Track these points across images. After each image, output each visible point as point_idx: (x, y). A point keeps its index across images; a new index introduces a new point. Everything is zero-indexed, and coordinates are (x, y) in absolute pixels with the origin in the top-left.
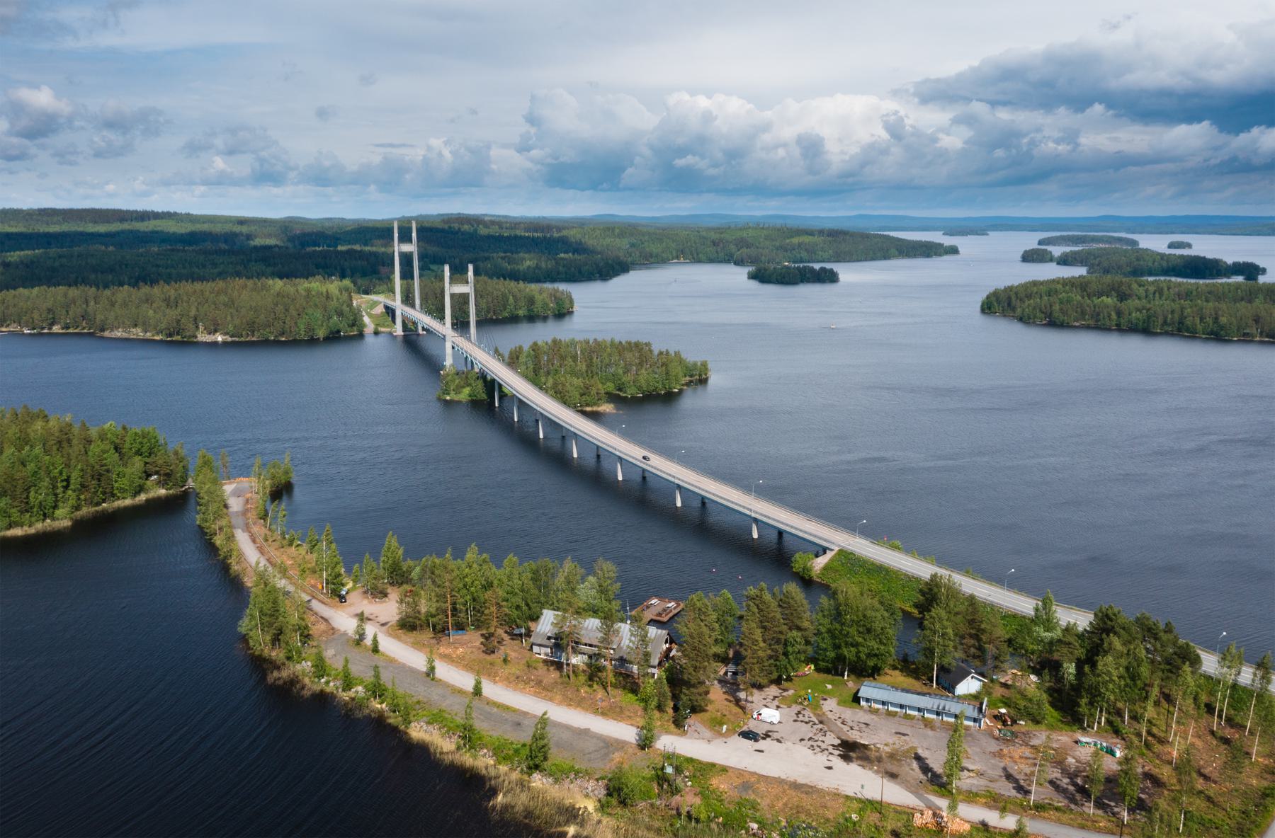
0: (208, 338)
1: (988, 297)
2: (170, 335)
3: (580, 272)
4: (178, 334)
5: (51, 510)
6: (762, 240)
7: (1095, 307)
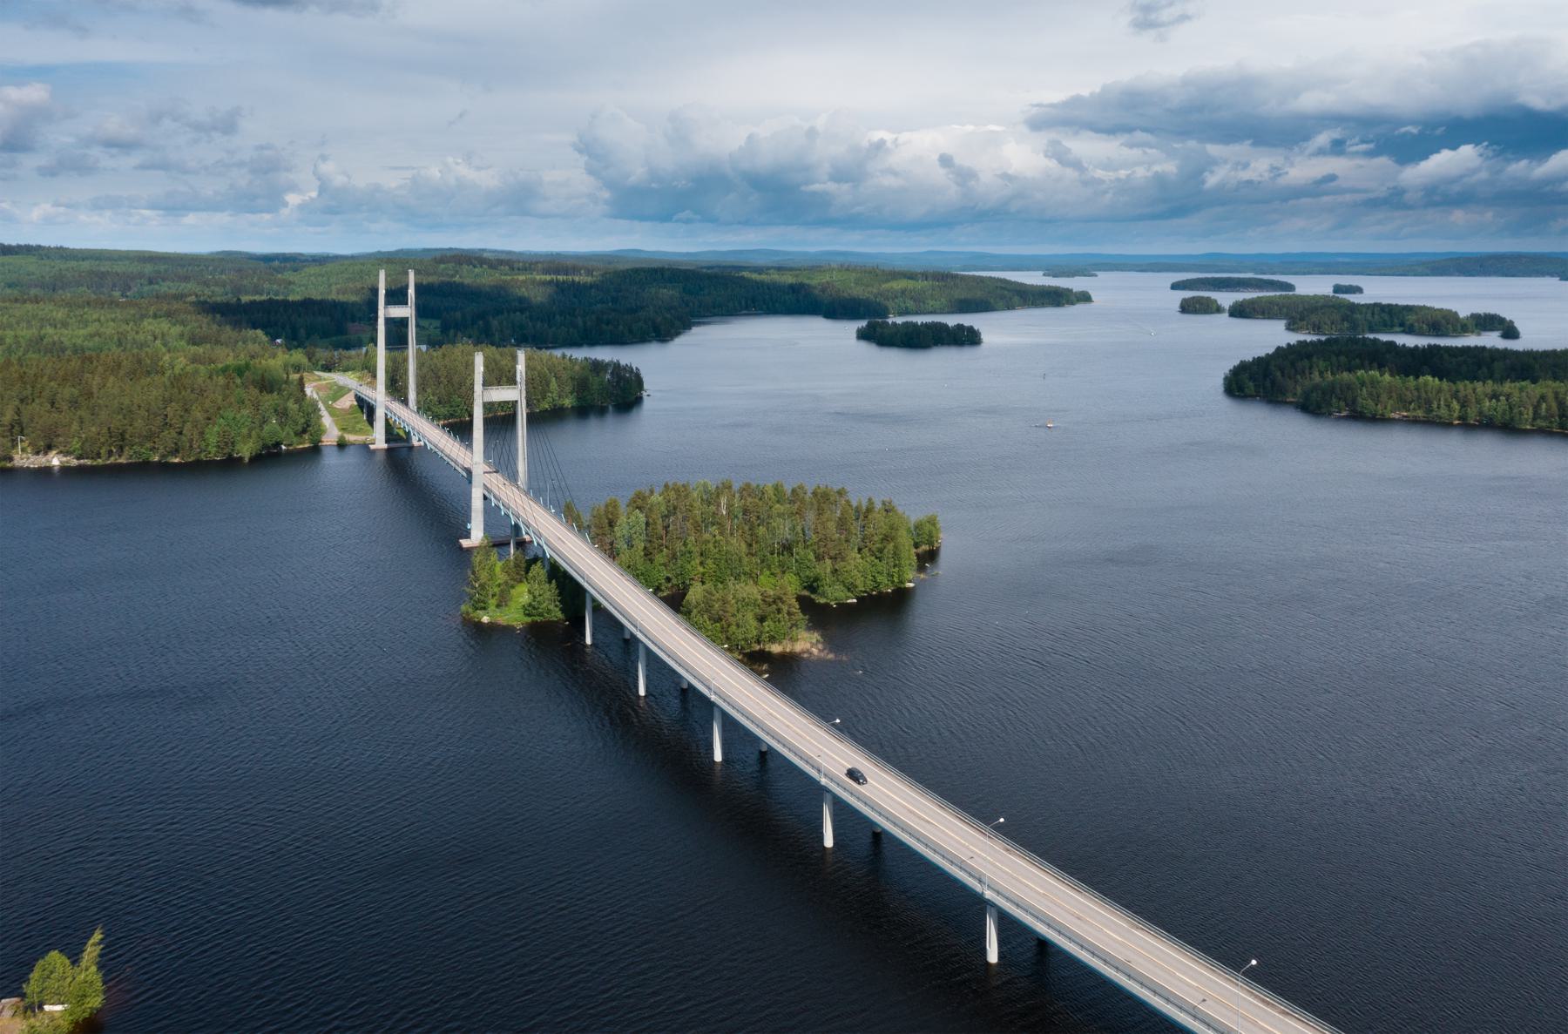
3: (631, 331)
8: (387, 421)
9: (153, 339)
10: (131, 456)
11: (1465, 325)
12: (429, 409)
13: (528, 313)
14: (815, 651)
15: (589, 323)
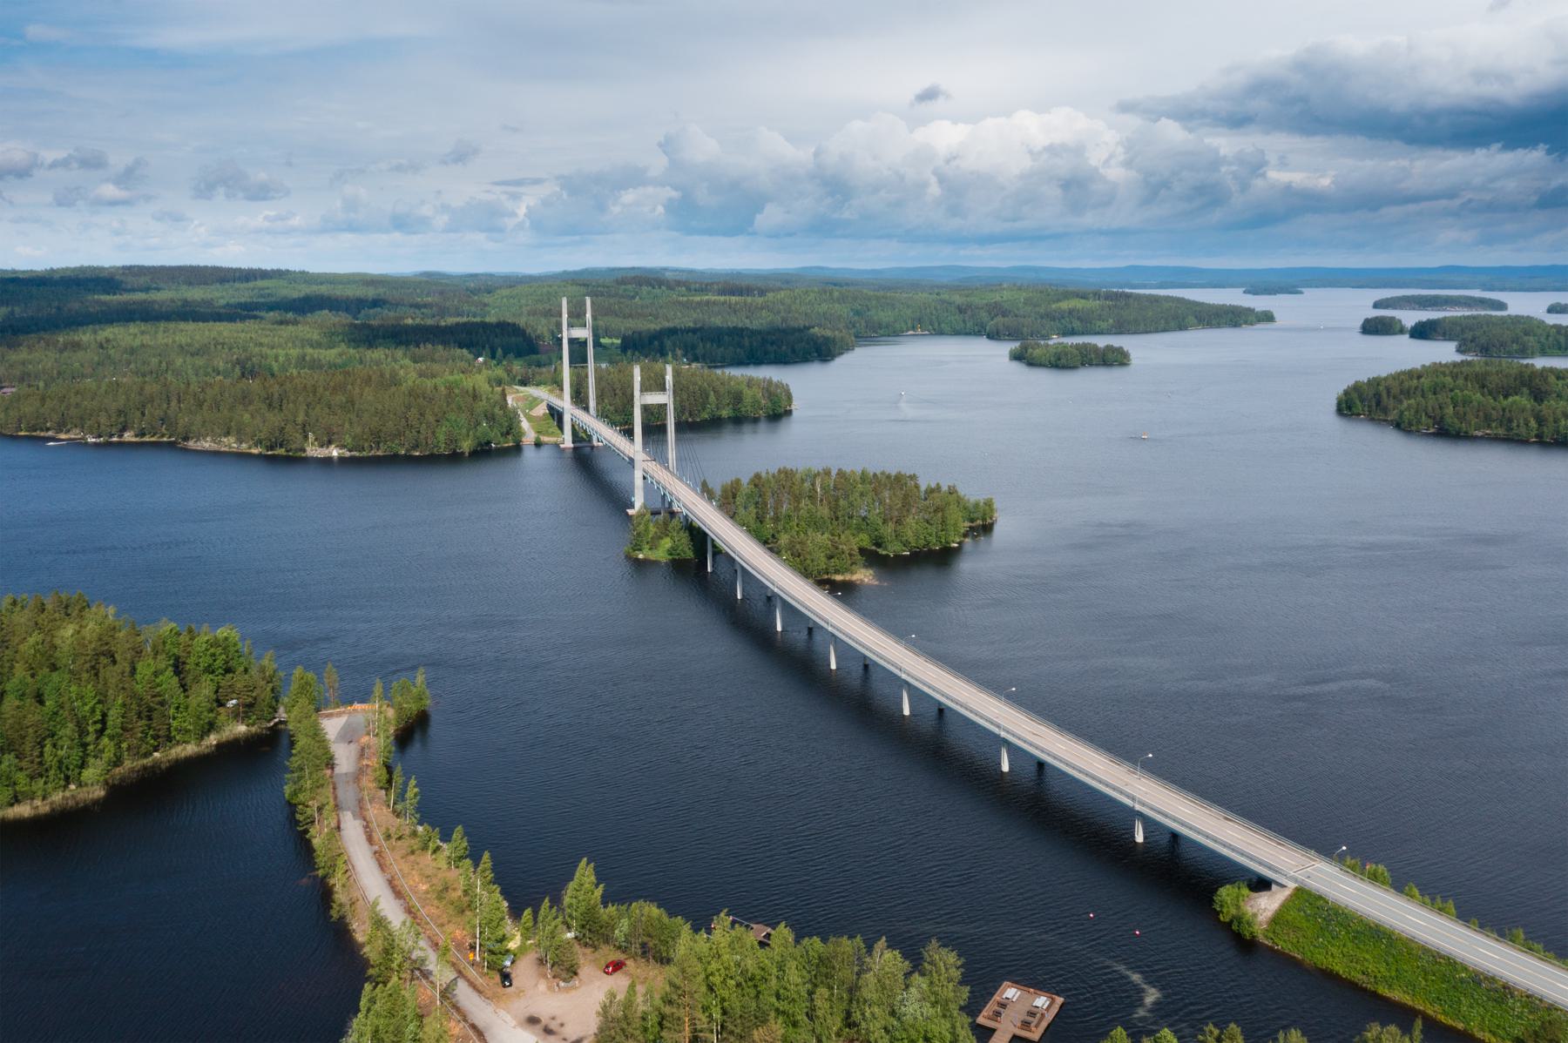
0: (320, 453)
1: (1346, 393)
2: (272, 448)
3: (794, 351)
4: (281, 446)
5: (77, 771)
6: (1021, 305)
7: (1504, 410)
8: (573, 426)
12: (607, 417)
14: (866, 580)
15: (755, 344)
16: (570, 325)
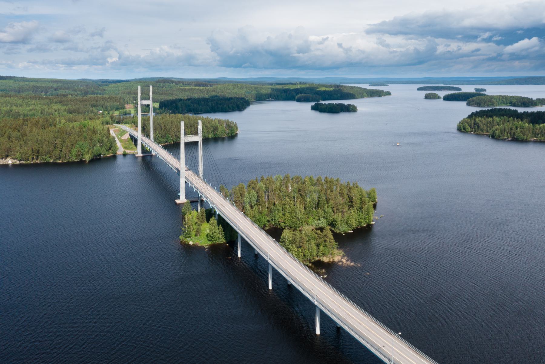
3: (229, 107)
8: (142, 145)
9: (54, 111)
10: (42, 160)
11: (536, 103)
13: (191, 101)
14: (344, 261)
15: (213, 105)
16: (142, 99)
